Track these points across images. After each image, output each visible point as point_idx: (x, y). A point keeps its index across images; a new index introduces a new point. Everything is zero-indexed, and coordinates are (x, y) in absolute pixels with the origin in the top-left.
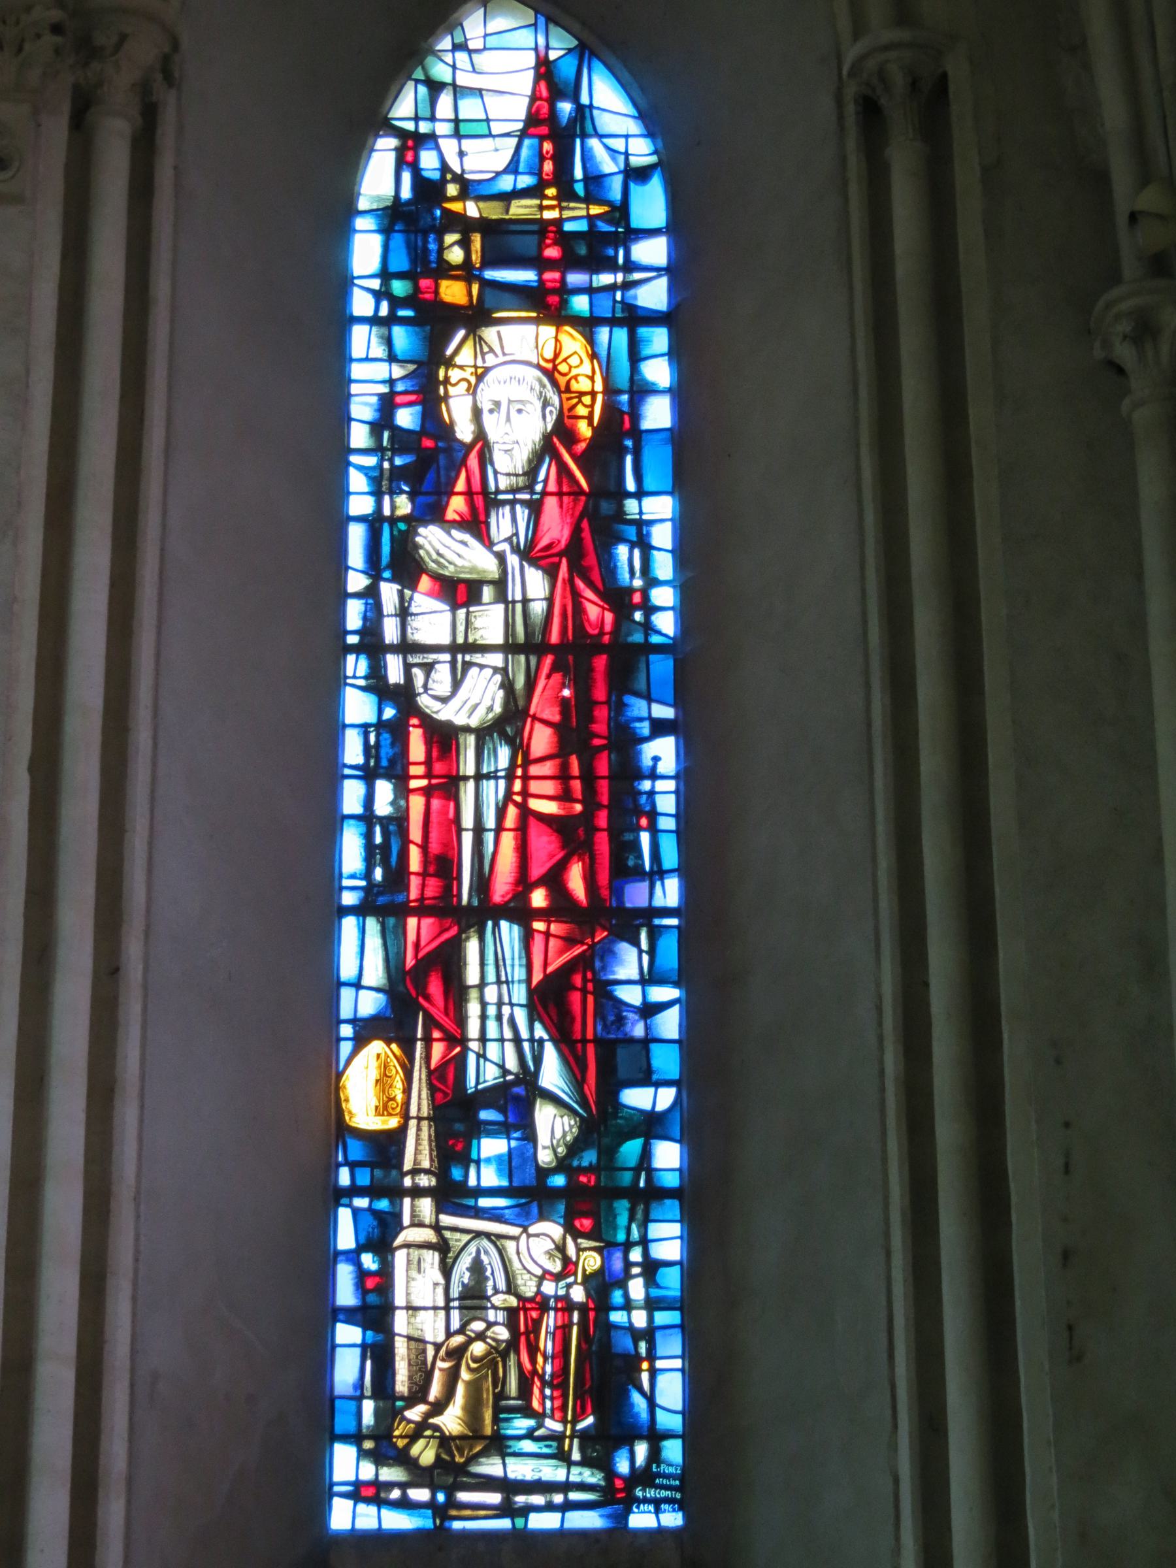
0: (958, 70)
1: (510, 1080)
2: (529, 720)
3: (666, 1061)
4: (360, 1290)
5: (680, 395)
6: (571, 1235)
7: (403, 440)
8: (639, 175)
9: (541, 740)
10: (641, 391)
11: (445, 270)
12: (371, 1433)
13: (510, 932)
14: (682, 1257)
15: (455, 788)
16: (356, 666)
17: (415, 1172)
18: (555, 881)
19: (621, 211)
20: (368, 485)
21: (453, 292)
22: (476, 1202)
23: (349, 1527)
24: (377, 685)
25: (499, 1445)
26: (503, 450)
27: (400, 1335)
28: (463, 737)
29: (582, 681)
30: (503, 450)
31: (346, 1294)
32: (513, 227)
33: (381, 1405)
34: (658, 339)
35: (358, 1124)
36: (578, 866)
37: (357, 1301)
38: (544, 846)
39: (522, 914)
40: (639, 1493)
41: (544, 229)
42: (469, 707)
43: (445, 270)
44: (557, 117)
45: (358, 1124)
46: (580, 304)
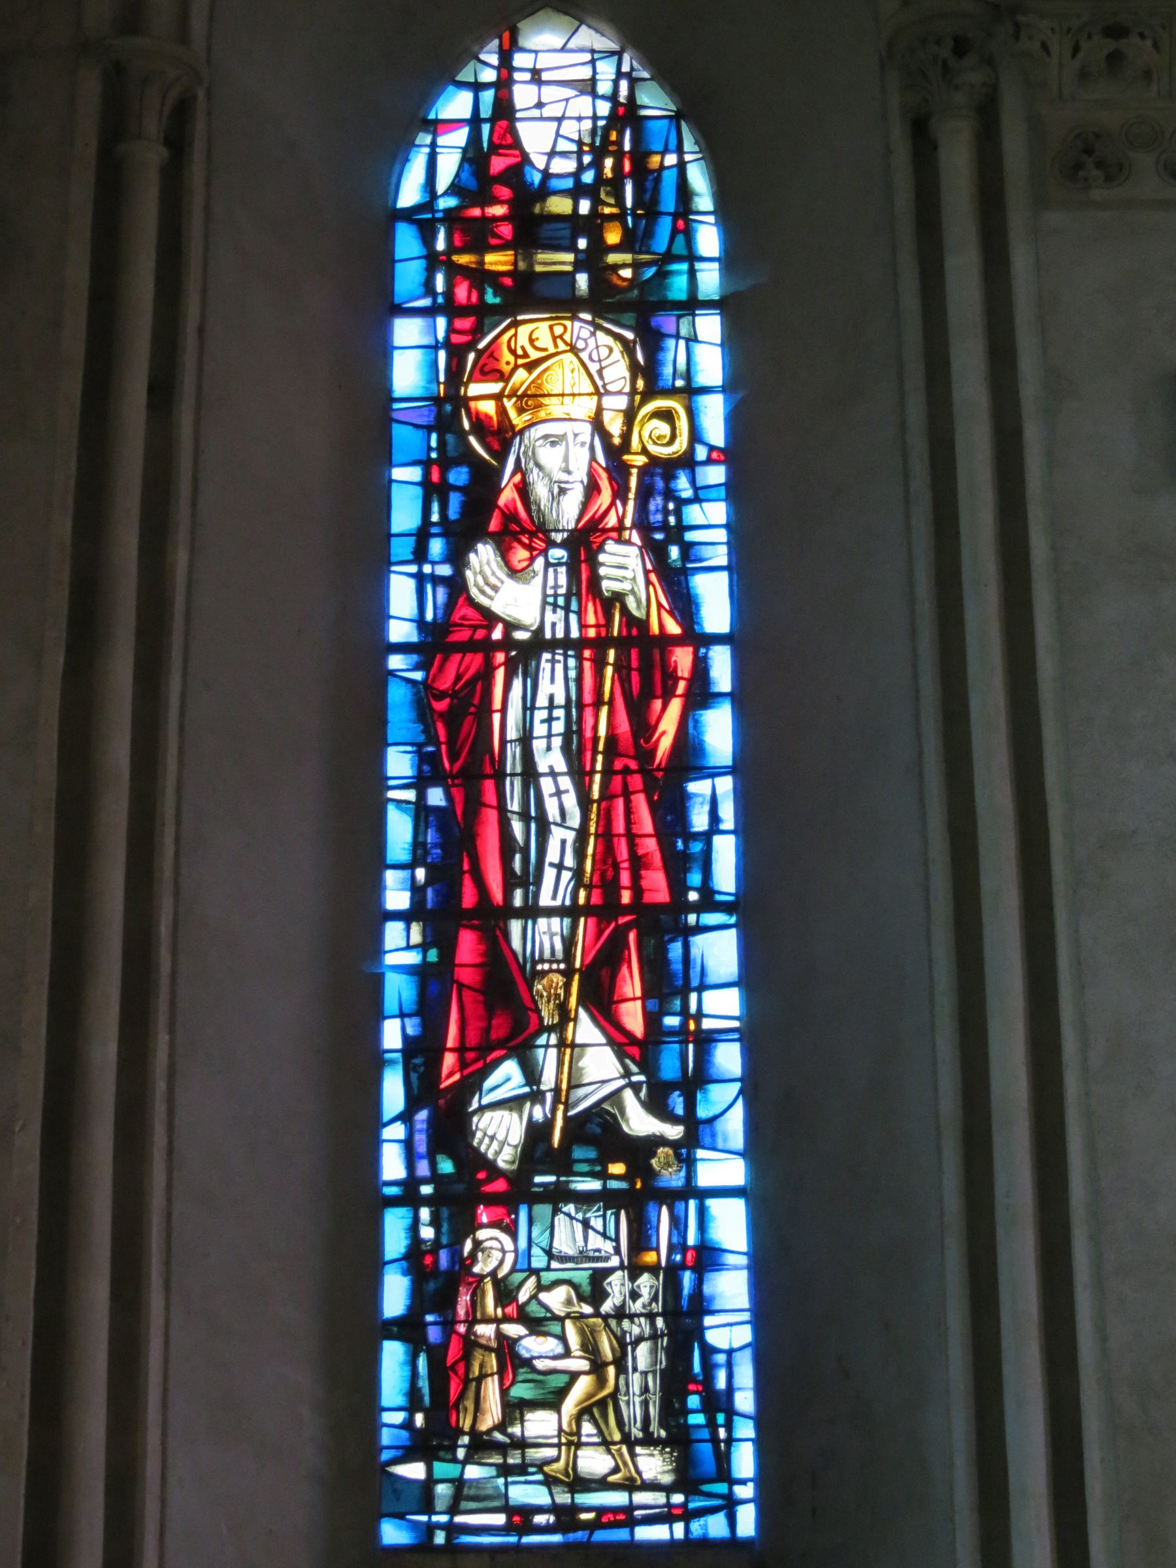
2: (626, 1263)
4: (428, 188)
6: (587, 1009)
12: (732, 406)
15: (470, 857)
17: (547, 1046)
20: (637, 1461)
22: (632, 1533)
23: (392, 612)
26: (719, 556)
27: (526, 1336)
28: (521, 1348)
30: (719, 556)
32: (503, 1533)
35: (614, 1064)
36: (494, 170)
37: (601, 901)
40: (639, 1482)
42: (587, 730)
44: (747, 1008)
45: (614, 1064)
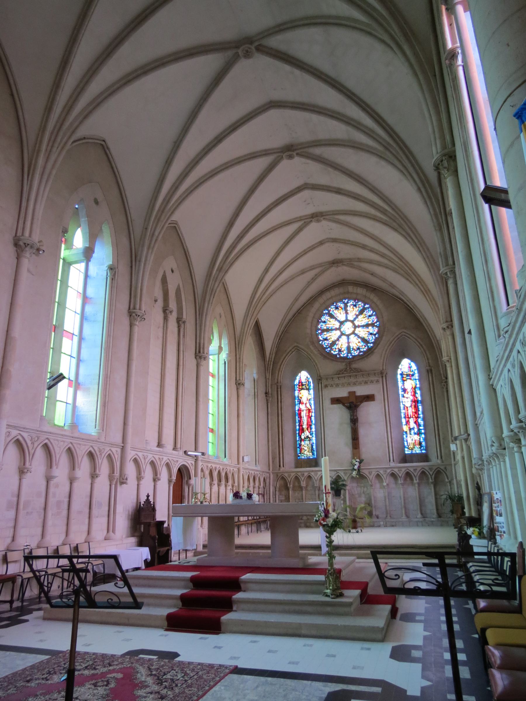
0: (433, 369)
1: (500, 183)
3: (422, 425)
5: (419, 384)
7: (403, 389)
8: (415, 370)
9: (413, 407)
10: (417, 384)
11: (404, 378)
13: (412, 418)
14: (78, 610)
16: (401, 403)
18: (415, 415)
19: (414, 373)
21: (405, 379)
24: (403, 405)
25: (414, 448)
29: (415, 403)
31: (405, 440)
33: (83, 219)
34: (417, 381)
38: (414, 414)
39: (413, 417)
41: (410, 374)
43: (404, 378)
46: (412, 379)
